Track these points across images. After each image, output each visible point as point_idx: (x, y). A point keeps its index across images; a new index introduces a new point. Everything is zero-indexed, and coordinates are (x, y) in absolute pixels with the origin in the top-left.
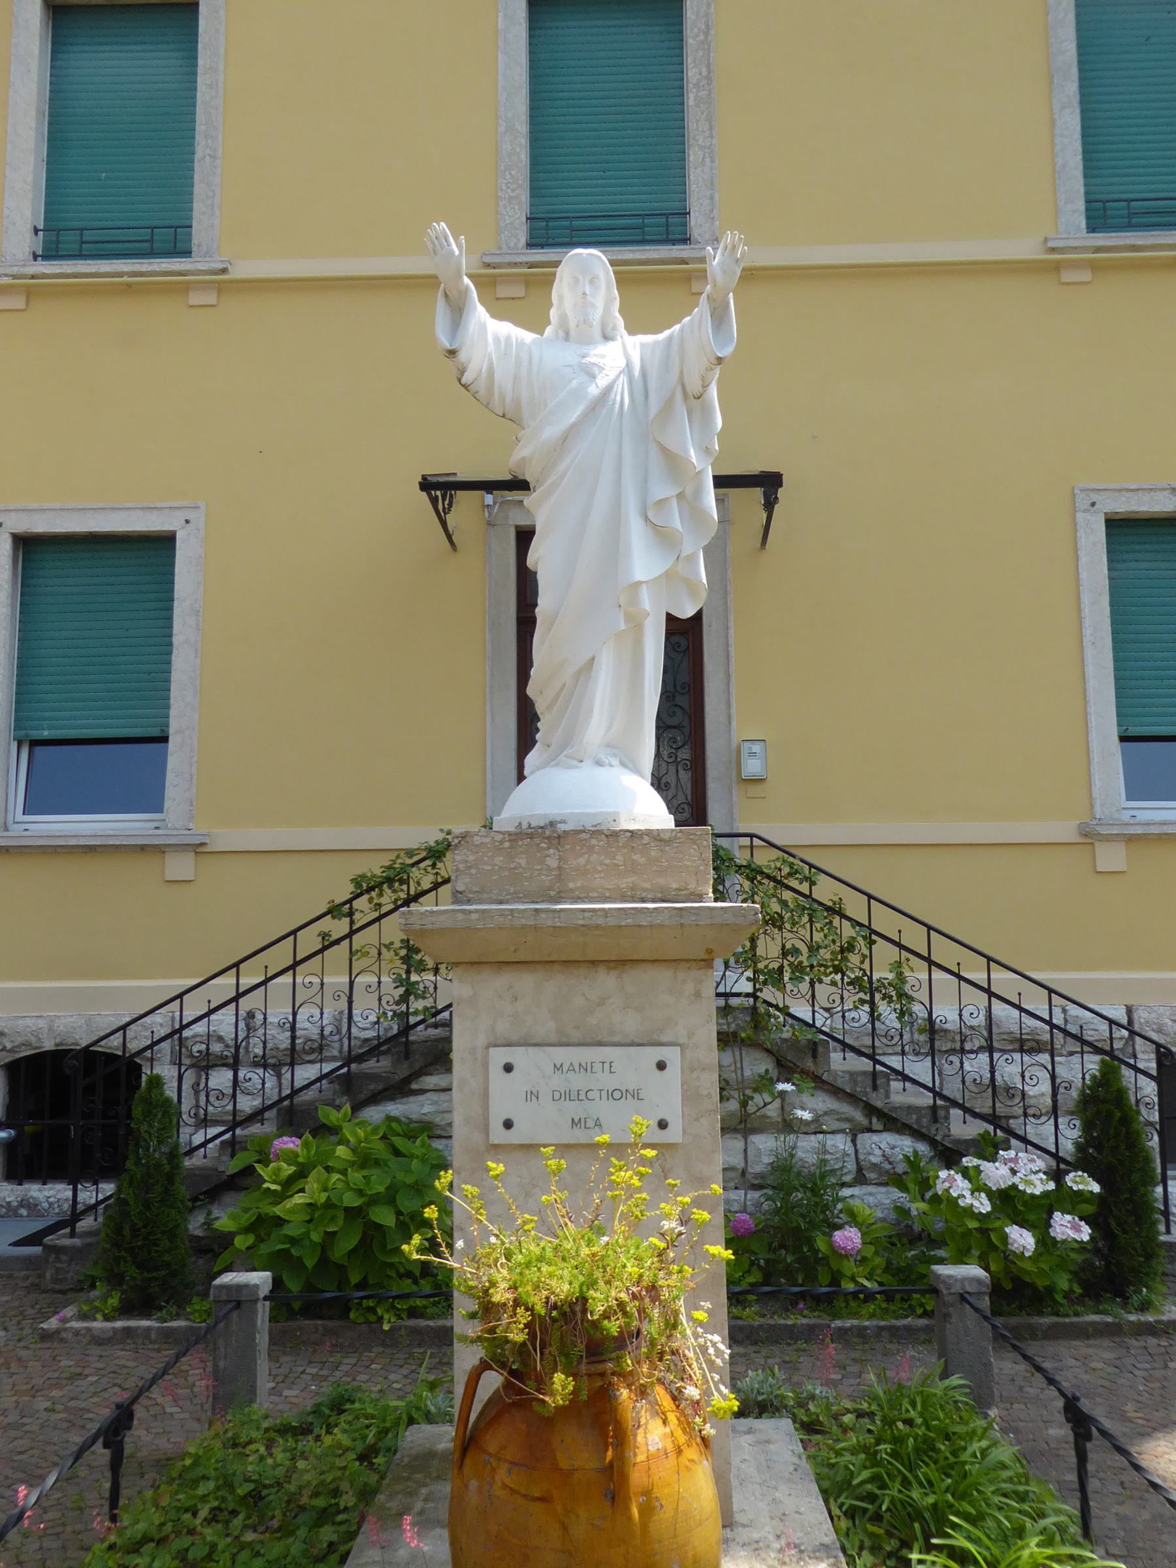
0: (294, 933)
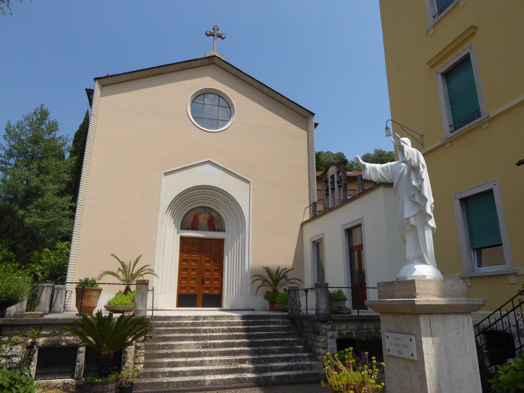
0: (512, 300)
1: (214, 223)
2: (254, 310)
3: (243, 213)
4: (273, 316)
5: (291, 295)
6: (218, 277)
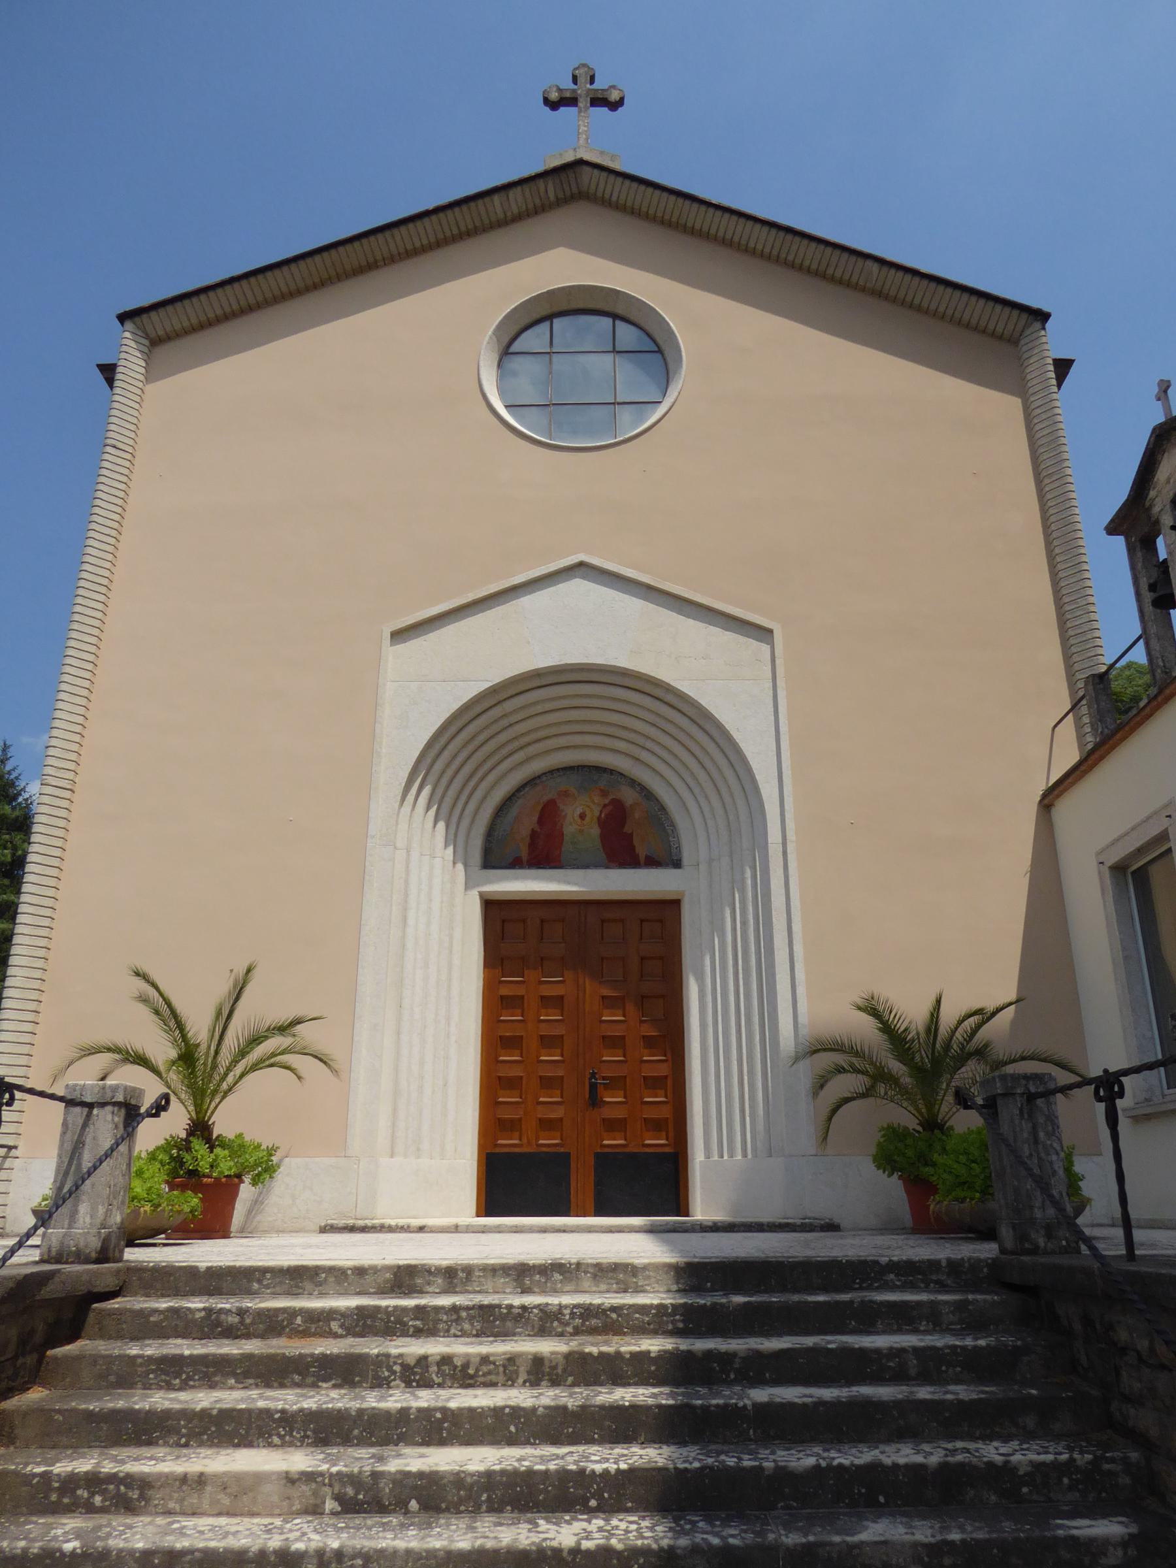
1: (632, 830)
2: (831, 1227)
3: (749, 770)
4: (893, 1267)
5: (1005, 1129)
6: (664, 1070)
